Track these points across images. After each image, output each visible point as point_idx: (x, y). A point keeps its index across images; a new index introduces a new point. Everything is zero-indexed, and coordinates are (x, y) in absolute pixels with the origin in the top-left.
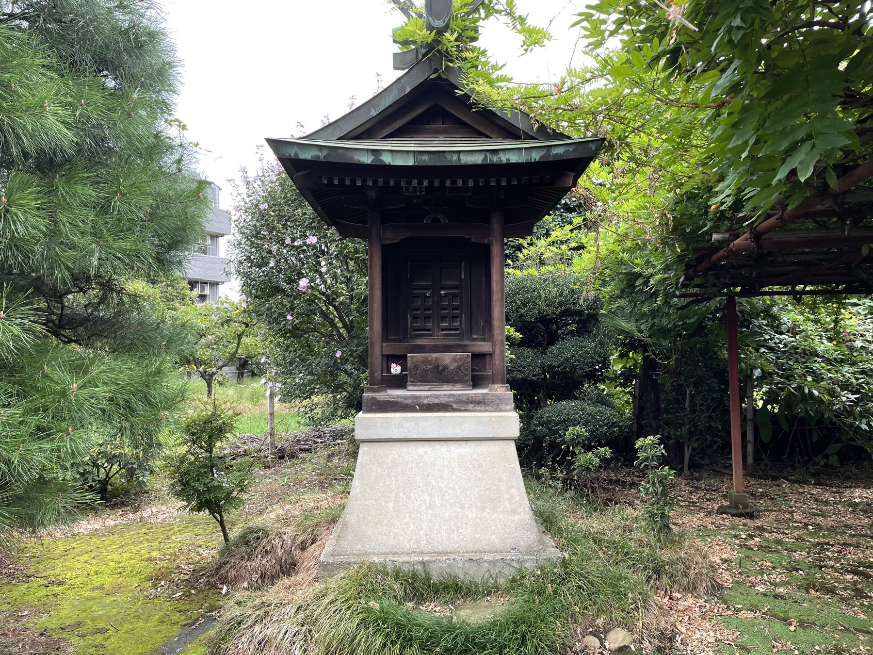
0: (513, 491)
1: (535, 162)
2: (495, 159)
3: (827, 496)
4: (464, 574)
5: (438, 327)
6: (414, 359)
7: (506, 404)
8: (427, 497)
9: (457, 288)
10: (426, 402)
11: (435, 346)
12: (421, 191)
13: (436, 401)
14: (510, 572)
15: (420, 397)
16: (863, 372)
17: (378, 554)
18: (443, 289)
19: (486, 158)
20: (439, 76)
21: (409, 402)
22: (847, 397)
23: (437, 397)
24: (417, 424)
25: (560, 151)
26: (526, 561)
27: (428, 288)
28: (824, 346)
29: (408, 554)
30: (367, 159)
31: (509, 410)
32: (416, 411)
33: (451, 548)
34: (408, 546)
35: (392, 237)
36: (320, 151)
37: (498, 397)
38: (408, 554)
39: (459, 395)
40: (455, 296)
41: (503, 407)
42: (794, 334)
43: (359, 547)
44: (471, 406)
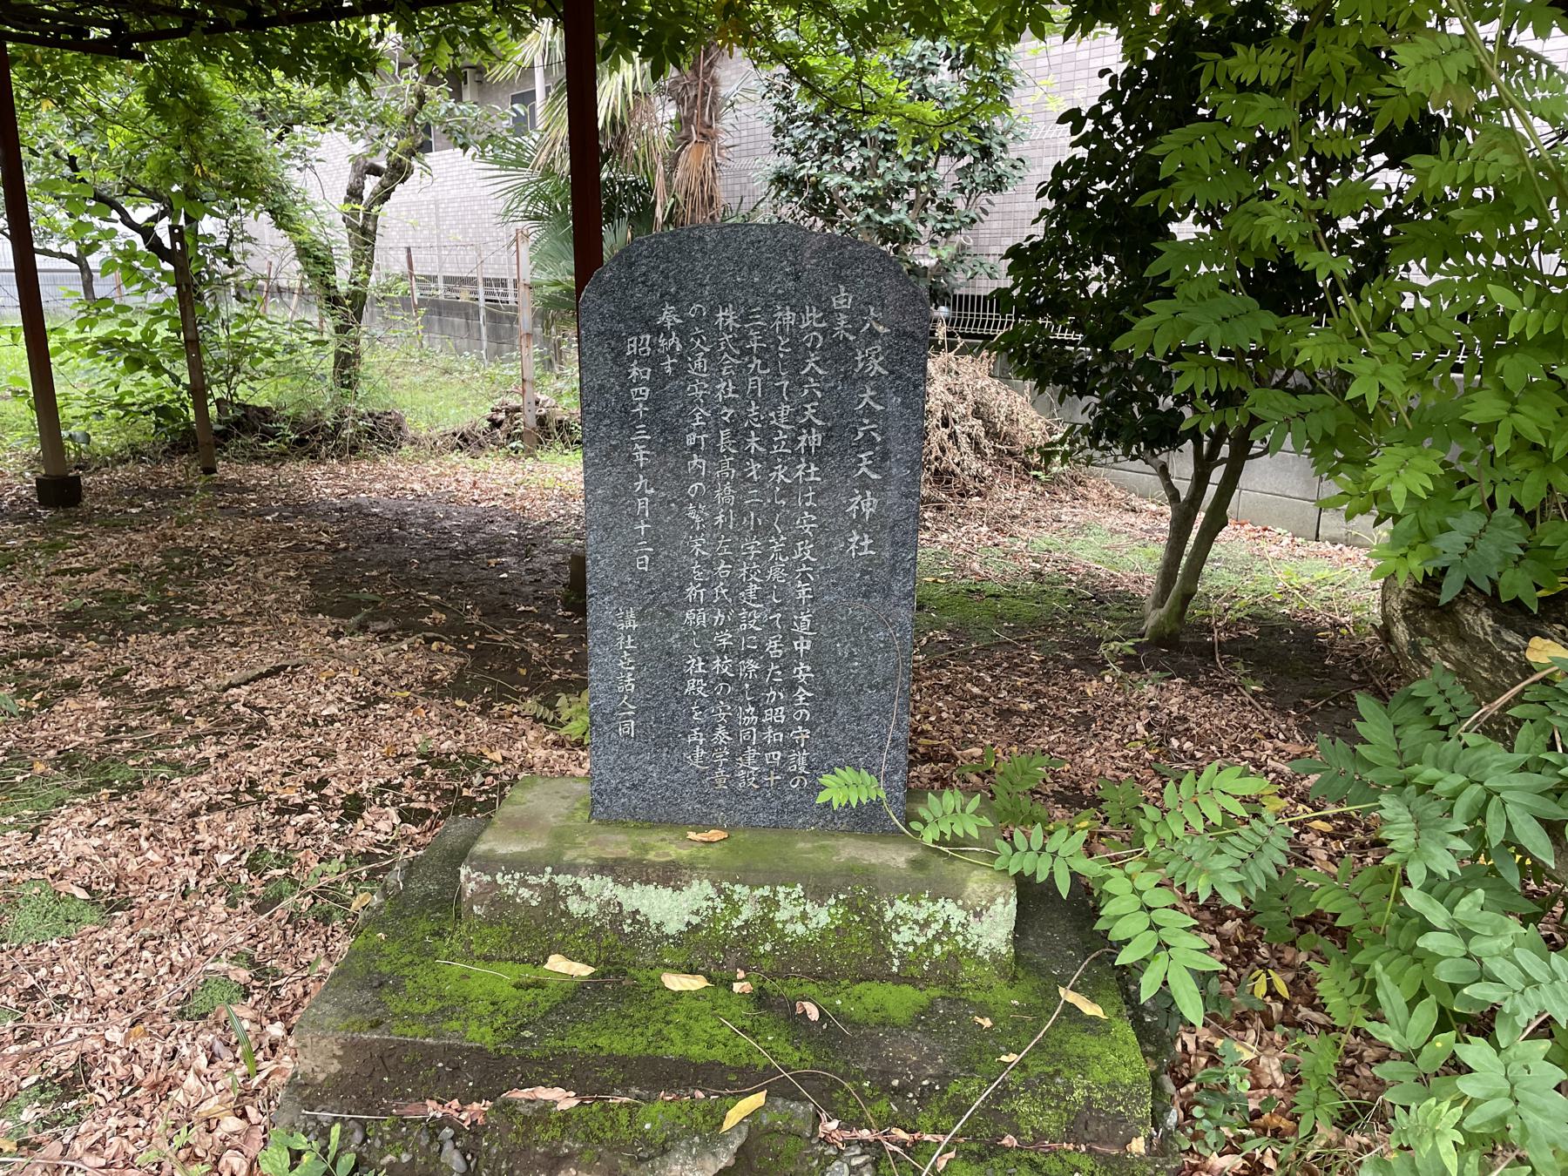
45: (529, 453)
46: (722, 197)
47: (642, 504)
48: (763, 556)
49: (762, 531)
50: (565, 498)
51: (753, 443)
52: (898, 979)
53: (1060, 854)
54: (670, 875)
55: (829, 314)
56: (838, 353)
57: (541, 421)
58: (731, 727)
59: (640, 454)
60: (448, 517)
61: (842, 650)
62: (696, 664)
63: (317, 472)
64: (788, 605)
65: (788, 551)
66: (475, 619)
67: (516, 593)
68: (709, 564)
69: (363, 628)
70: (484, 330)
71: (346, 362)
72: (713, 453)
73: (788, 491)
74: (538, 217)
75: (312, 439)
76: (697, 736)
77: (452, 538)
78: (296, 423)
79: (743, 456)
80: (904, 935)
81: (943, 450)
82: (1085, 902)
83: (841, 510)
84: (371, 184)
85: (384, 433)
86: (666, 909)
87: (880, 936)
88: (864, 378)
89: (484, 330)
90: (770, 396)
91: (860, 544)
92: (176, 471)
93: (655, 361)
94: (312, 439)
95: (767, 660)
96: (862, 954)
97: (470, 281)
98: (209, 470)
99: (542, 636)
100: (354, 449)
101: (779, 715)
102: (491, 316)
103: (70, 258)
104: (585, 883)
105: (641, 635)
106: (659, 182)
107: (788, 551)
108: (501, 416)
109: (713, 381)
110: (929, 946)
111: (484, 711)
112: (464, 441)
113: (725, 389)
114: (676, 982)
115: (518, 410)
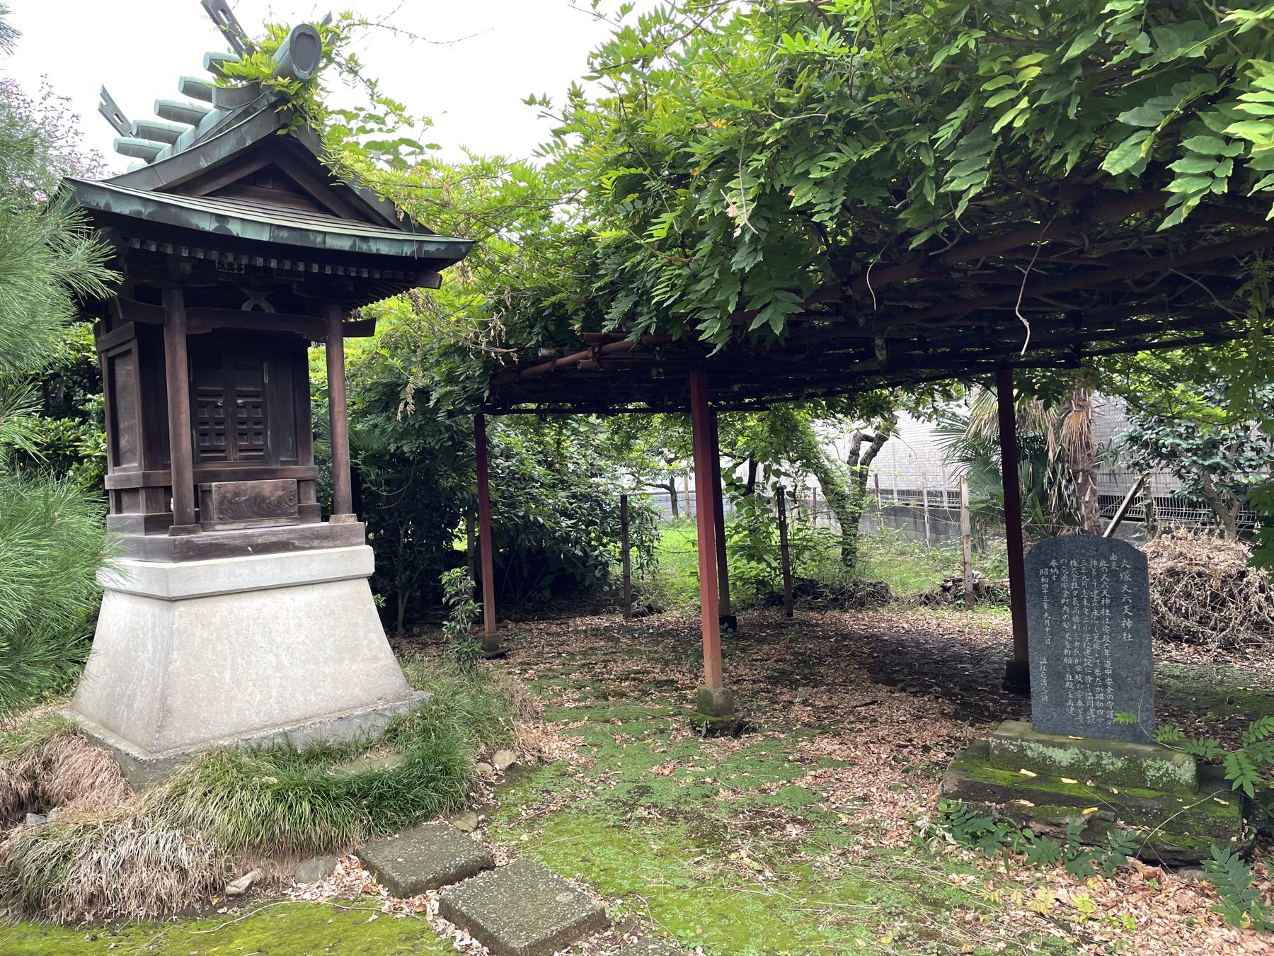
0: (372, 636)
1: (406, 257)
2: (364, 247)
3: (554, 629)
4: (348, 734)
5: (236, 445)
6: (223, 490)
7: (357, 536)
8: (272, 658)
9: (258, 396)
10: (260, 541)
11: (234, 472)
12: (240, 269)
13: (274, 539)
14: (383, 723)
15: (253, 536)
16: (574, 496)
17: (223, 737)
18: (240, 395)
19: (354, 244)
20: (288, 135)
21: (238, 542)
22: (566, 523)
23: (274, 534)
24: (254, 570)
25: (432, 248)
26: (398, 707)
27: (219, 395)
28: (539, 471)
29: (258, 729)
30: (209, 226)
31: (360, 544)
32: (248, 554)
33: (310, 713)
34: (256, 721)
35: (205, 328)
36: (144, 206)
37: (347, 528)
38: (258, 729)
39: (302, 530)
40: (256, 406)
41: (354, 540)
42: (508, 458)
43: (192, 734)
44: (316, 542)
45: (969, 608)
46: (1095, 441)
47: (1047, 622)
48: (1091, 640)
49: (1091, 632)
50: (996, 634)
51: (1085, 602)
52: (1149, 788)
53: (1210, 748)
54: (1062, 746)
55: (1109, 562)
56: (1113, 574)
57: (976, 587)
58: (1083, 700)
59: (1046, 606)
60: (927, 642)
61: (1124, 674)
62: (1068, 677)
63: (846, 616)
64: (1102, 658)
65: (1100, 638)
66: (957, 690)
67: (976, 682)
68: (1072, 642)
69: (903, 690)
70: (927, 526)
71: (849, 554)
72: (1071, 606)
73: (1099, 618)
74: (968, 459)
75: (842, 598)
76: (1070, 703)
77: (933, 654)
78: (833, 591)
79: (1081, 608)
80: (1151, 773)
81: (1260, 608)
82: (1218, 761)
83: (1119, 625)
84: (865, 447)
85: (880, 595)
86: (1063, 757)
87: (1141, 772)
88: (1124, 582)
89: (927, 526)
90: (1091, 588)
91: (1127, 637)
92: (774, 614)
93: (1050, 576)
94: (842, 598)
95: (1095, 677)
96: (1134, 775)
97: (920, 493)
98: (790, 615)
99: (993, 700)
100: (862, 604)
101: (1101, 696)
102: (932, 513)
103: (665, 487)
104: (1033, 745)
105: (1048, 666)
106: (1051, 438)
107: (1100, 638)
108: (950, 584)
109: (1070, 582)
110: (1161, 777)
111: (972, 725)
112: (928, 600)
113: (1074, 585)
114: (1066, 781)
115: (960, 580)
